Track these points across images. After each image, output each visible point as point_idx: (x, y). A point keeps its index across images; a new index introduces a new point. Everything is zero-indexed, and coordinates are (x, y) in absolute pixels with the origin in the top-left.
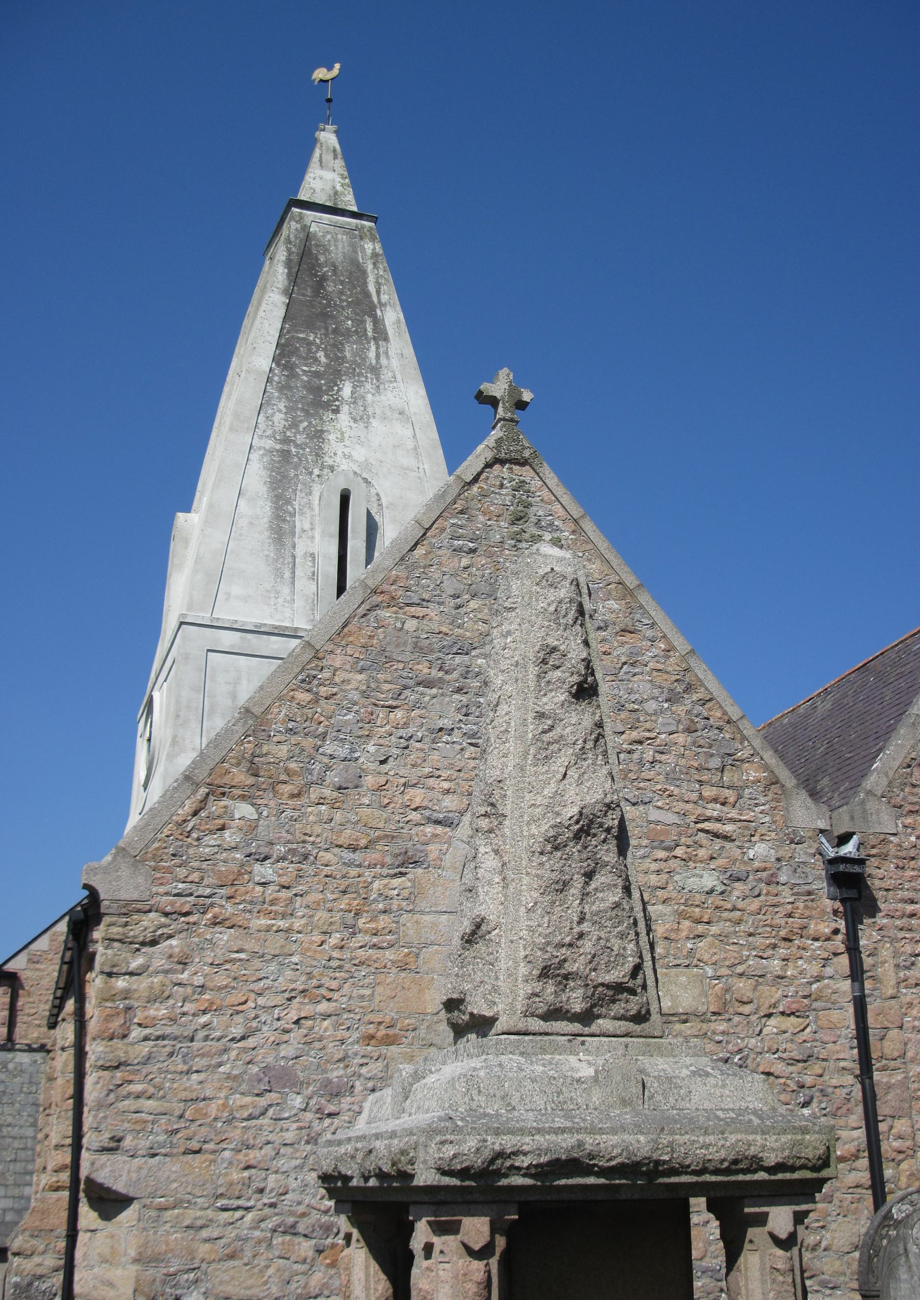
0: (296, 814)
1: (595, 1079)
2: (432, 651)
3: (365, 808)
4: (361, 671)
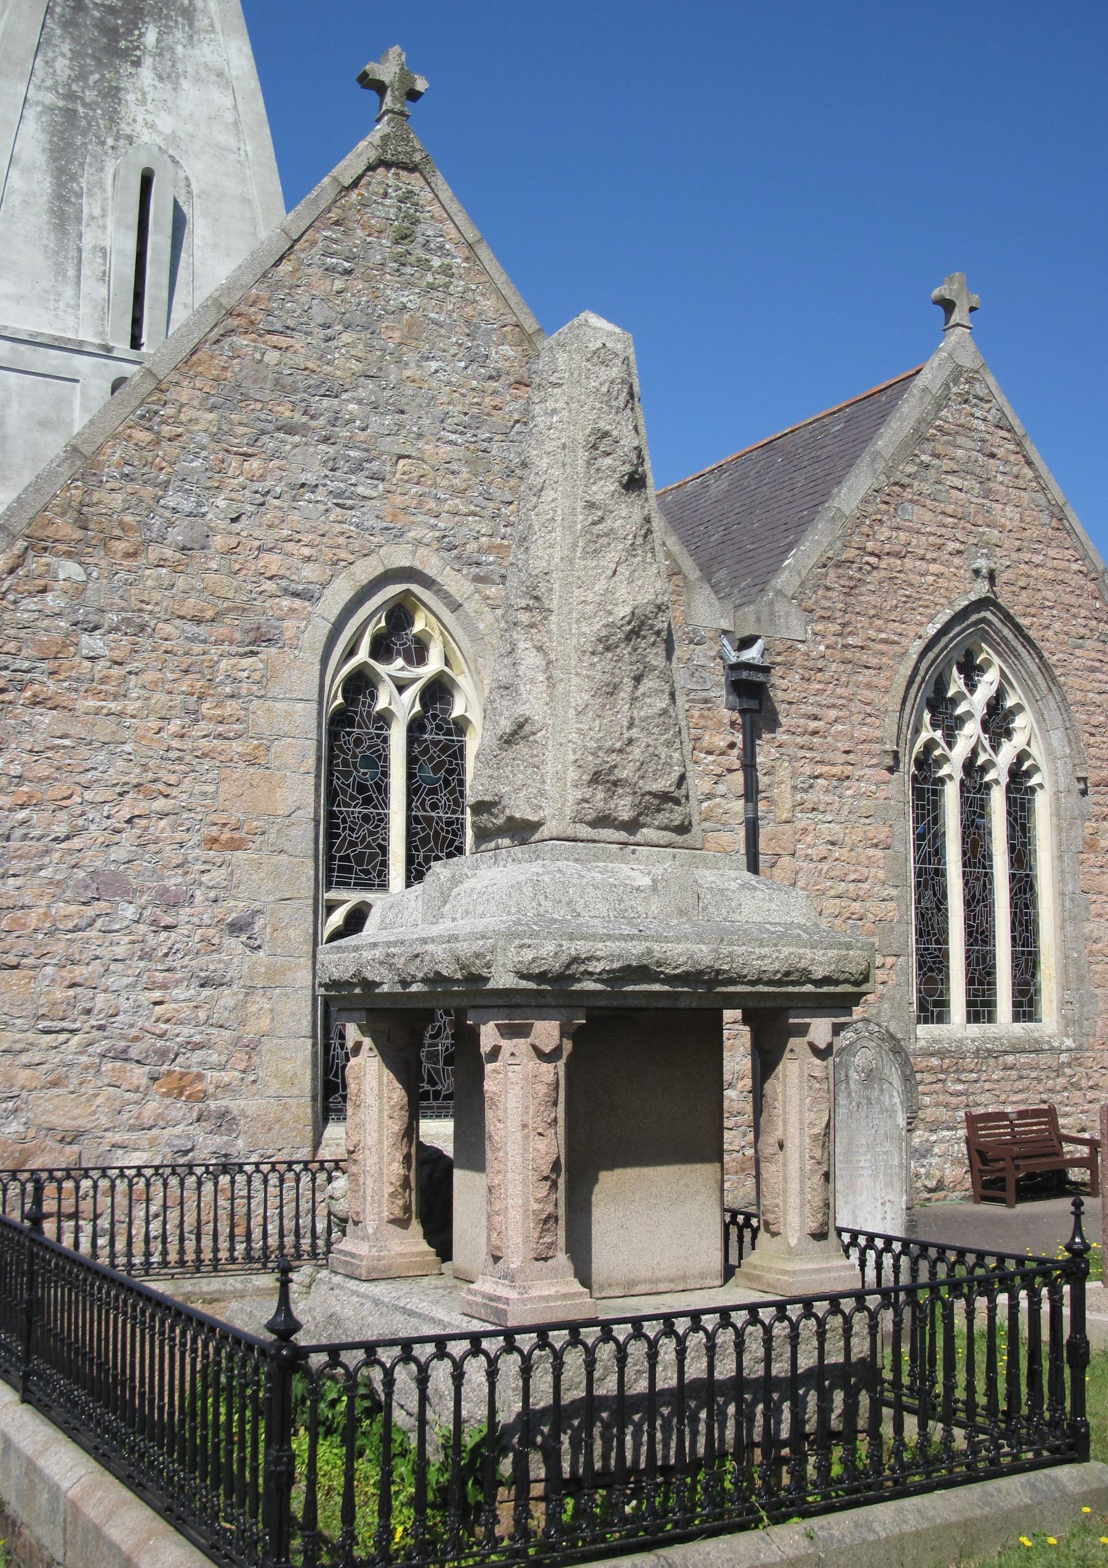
0: (132, 577)
1: (654, 889)
2: (296, 391)
3: (212, 574)
4: (212, 409)
